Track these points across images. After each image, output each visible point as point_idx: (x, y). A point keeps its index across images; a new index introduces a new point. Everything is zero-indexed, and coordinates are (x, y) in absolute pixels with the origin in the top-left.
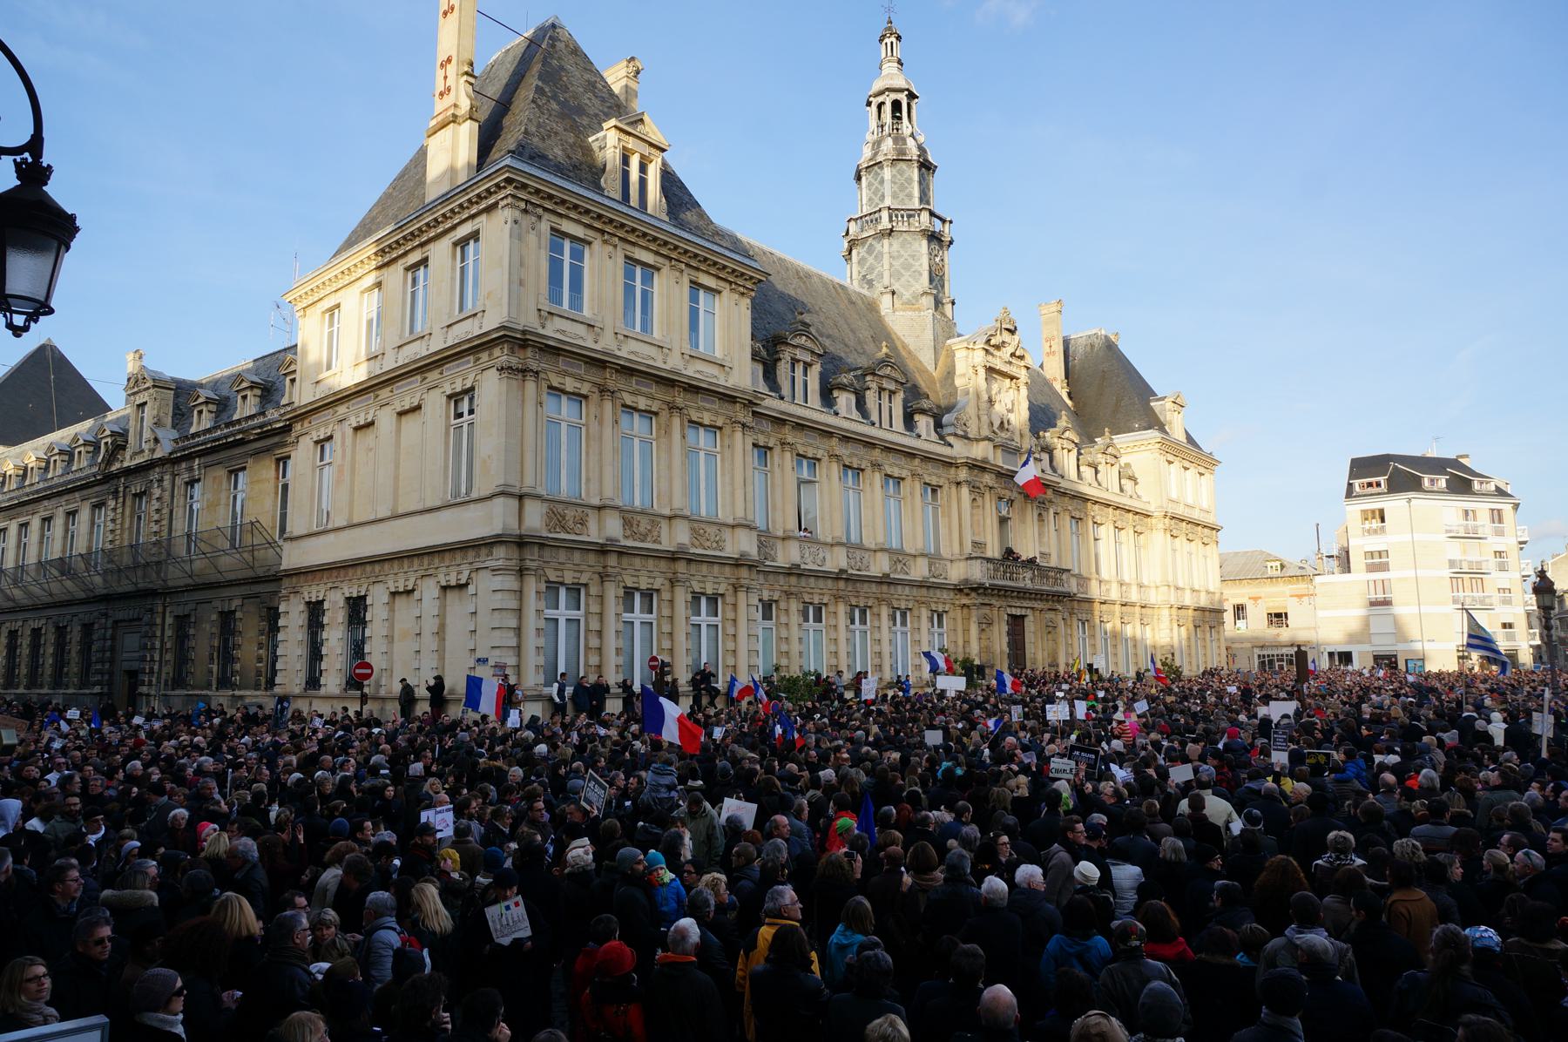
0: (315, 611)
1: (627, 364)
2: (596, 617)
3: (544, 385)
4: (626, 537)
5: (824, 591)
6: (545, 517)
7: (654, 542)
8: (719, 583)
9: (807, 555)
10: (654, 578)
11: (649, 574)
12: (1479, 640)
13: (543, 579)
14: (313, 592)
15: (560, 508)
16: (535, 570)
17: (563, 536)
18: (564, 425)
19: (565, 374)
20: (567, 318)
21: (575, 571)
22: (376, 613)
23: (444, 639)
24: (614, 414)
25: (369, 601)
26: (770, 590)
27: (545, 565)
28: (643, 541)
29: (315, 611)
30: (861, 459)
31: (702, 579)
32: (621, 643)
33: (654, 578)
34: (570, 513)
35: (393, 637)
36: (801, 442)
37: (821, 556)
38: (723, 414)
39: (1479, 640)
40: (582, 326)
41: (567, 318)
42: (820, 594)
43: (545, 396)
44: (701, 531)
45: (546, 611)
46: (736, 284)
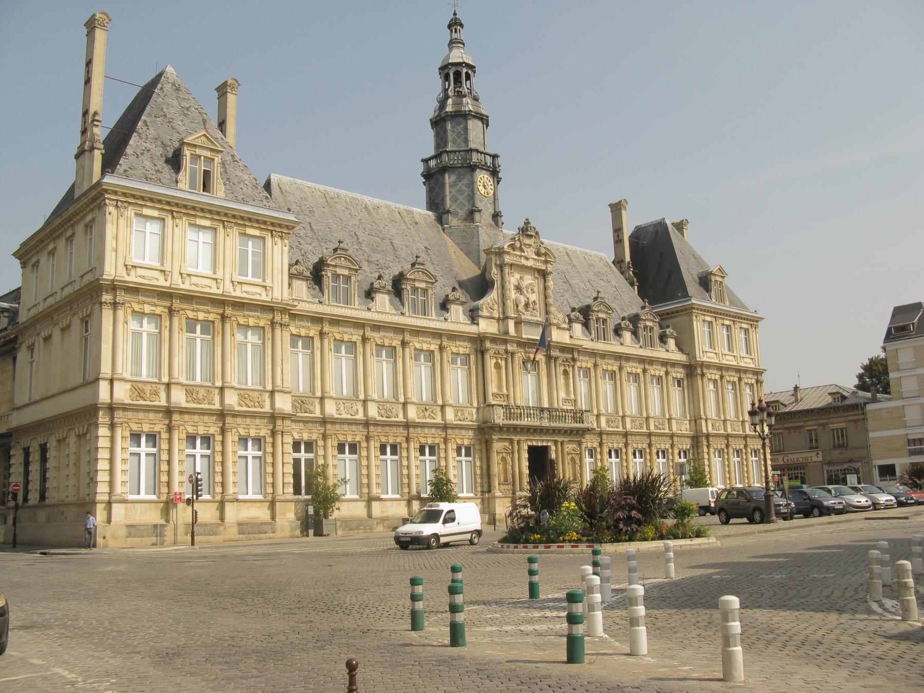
0: (27, 452)
1: (186, 293)
2: (322, 458)
3: (129, 311)
4: (187, 401)
5: (356, 433)
6: (129, 391)
7: (209, 404)
8: (435, 438)
9: (342, 408)
10: (260, 429)
11: (204, 425)
12: (166, 536)
13: (237, 434)
14: (25, 442)
15: (140, 385)
16: (122, 424)
17: (141, 402)
18: (249, 346)
19: (144, 303)
20: (146, 268)
21: (150, 424)
22: (51, 454)
23: (79, 467)
24: (126, 317)
25: (48, 446)
26: (309, 433)
27: (129, 421)
28: (200, 404)
29: (27, 452)
30: (392, 339)
31: (462, 437)
32: (418, 472)
33: (260, 429)
34: (148, 389)
35: (59, 468)
36: (337, 331)
37: (354, 409)
38: (263, 318)
39: (166, 536)
40: (210, 280)
41: (146, 268)
42: (353, 435)
43: (130, 318)
44: (247, 396)
45: (187, 450)
46: (276, 231)
